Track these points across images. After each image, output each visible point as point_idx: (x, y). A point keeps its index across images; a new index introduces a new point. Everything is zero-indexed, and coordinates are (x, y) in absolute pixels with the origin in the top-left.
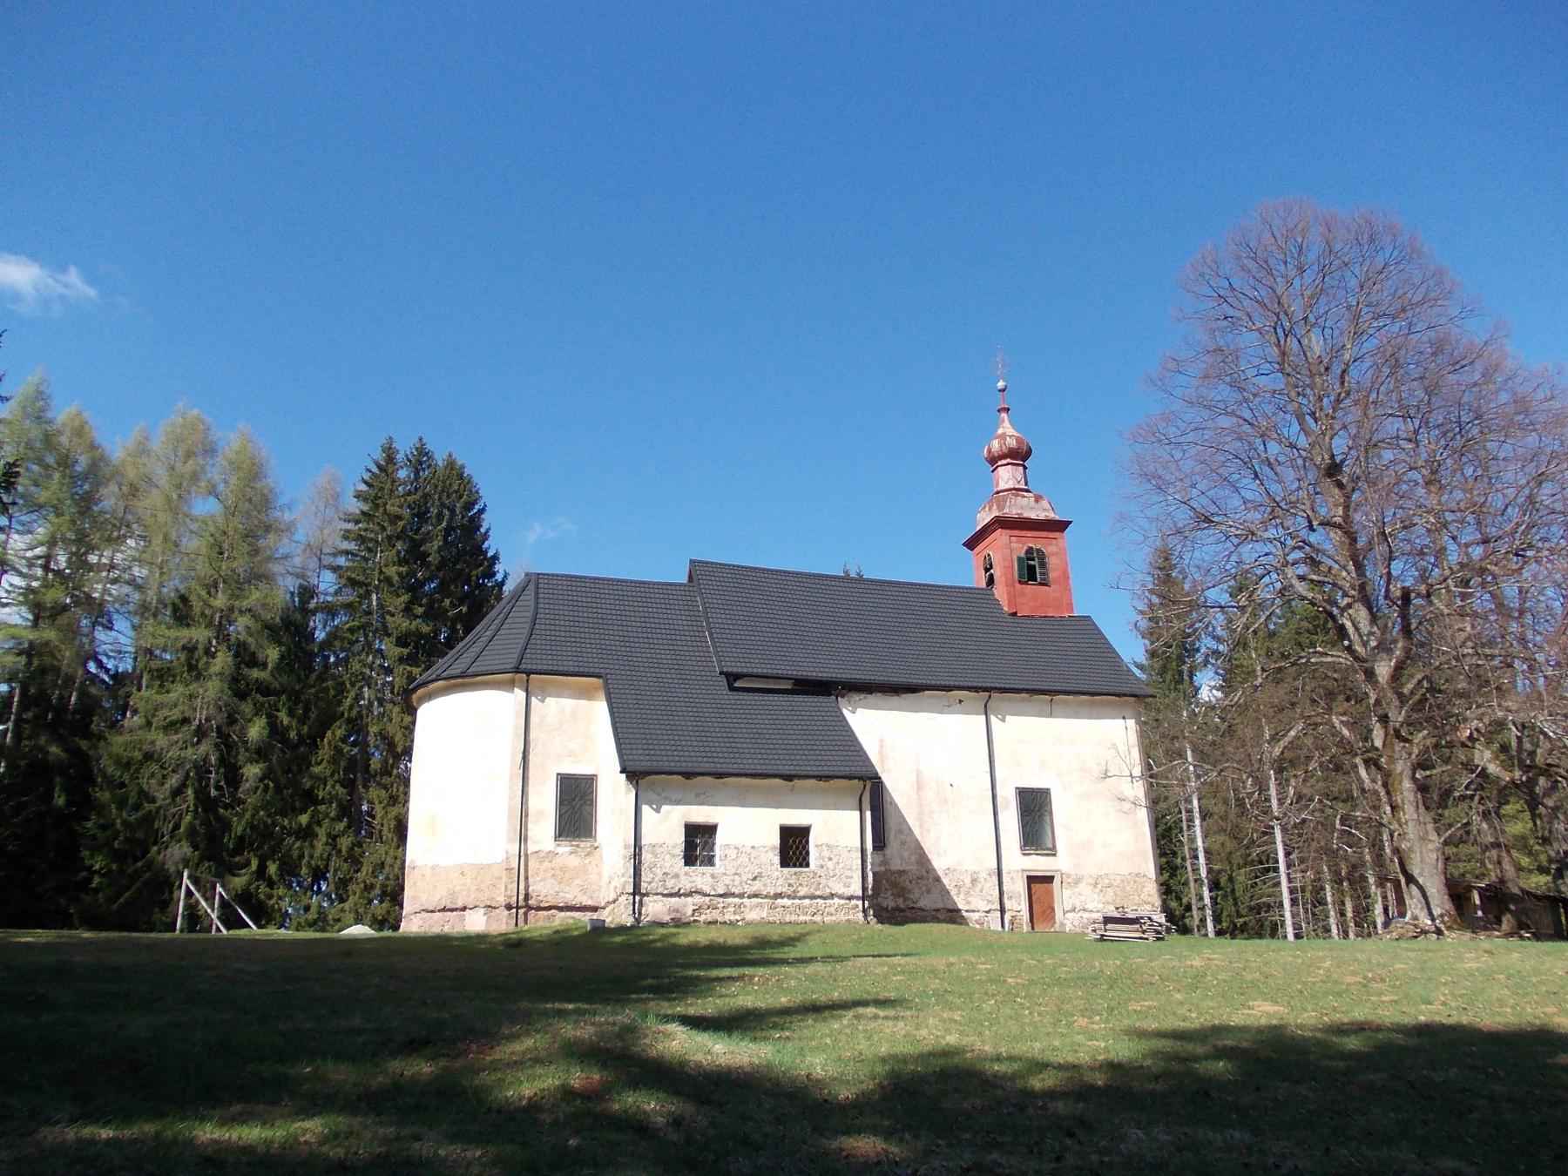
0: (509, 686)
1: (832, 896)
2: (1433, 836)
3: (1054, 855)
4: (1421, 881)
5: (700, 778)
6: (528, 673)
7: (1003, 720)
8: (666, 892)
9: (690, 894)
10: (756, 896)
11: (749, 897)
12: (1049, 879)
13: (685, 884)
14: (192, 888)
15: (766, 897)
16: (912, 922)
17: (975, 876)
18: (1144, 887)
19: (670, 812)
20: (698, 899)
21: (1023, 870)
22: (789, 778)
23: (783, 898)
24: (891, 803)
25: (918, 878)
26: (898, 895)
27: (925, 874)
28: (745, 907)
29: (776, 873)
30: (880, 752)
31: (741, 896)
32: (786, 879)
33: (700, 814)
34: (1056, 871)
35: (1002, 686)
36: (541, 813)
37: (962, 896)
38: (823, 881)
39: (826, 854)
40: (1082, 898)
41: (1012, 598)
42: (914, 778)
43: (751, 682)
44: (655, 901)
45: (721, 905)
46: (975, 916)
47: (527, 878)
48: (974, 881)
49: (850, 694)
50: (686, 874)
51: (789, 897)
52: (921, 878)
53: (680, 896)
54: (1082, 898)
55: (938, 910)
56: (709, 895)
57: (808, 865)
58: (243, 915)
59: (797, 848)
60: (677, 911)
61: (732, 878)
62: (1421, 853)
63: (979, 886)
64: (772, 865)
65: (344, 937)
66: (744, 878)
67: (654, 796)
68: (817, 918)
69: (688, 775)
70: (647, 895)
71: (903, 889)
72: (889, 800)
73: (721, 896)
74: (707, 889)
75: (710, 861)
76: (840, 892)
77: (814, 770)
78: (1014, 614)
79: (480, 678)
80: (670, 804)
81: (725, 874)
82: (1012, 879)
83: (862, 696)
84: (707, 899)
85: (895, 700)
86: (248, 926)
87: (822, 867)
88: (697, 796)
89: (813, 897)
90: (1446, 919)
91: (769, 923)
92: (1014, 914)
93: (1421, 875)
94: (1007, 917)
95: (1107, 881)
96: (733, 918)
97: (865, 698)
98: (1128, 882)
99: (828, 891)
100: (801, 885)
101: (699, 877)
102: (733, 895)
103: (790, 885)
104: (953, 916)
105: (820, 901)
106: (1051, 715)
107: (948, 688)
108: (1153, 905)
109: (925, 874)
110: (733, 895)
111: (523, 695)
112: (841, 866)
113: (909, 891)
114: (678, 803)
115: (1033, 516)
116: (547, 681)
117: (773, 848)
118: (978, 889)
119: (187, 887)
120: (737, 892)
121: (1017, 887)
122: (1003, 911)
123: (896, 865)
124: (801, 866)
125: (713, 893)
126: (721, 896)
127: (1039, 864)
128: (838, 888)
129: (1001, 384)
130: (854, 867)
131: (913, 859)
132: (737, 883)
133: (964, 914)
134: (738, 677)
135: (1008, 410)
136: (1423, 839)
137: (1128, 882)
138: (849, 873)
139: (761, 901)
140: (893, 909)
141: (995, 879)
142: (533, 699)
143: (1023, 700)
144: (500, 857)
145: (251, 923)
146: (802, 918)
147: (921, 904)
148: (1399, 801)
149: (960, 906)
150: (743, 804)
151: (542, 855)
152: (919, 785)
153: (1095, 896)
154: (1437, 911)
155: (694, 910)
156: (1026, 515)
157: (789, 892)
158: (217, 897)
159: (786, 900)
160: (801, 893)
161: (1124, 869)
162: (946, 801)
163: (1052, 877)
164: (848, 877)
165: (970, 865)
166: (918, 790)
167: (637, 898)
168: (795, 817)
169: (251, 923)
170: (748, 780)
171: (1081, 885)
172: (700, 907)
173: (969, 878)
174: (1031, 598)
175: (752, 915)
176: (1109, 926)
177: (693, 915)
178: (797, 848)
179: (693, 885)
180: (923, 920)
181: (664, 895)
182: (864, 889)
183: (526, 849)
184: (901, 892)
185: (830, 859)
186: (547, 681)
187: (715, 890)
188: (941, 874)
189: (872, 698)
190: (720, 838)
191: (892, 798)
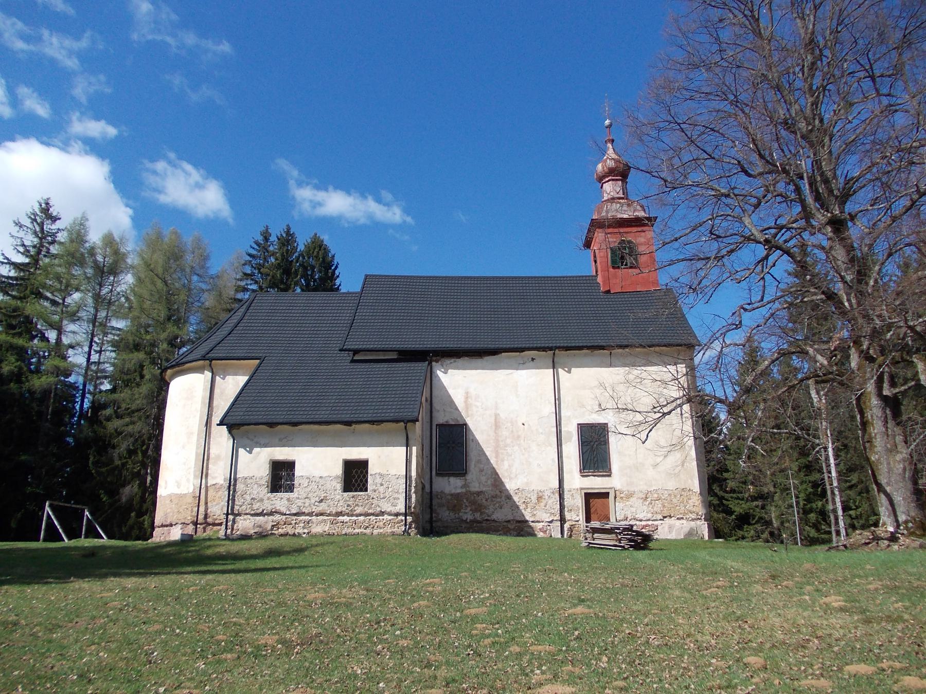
0: (200, 370)
1: (382, 513)
2: (901, 446)
3: (610, 476)
4: (888, 489)
5: (246, 427)
6: (211, 360)
7: (569, 372)
8: (252, 512)
9: (271, 513)
10: (322, 514)
11: (317, 515)
12: (606, 495)
13: (267, 506)
14: (50, 513)
15: (329, 515)
16: (453, 532)
17: (541, 494)
18: (690, 499)
19: (259, 453)
20: (277, 517)
21: (582, 489)
22: (348, 423)
23: (344, 516)
24: (473, 440)
25: (493, 497)
26: (475, 511)
27: (499, 494)
28: (313, 523)
29: (338, 497)
30: (466, 402)
31: (310, 514)
32: (346, 501)
33: (282, 453)
34: (611, 488)
35: (566, 345)
36: (218, 457)
37: (529, 510)
38: (375, 501)
39: (379, 480)
40: (633, 510)
41: (607, 280)
42: (492, 420)
43: (365, 355)
44: (245, 519)
45: (293, 522)
46: (540, 525)
47: (206, 503)
48: (539, 498)
49: (443, 359)
50: (268, 499)
51: (348, 515)
52: (496, 496)
53: (264, 515)
54: (633, 510)
55: (508, 521)
56: (285, 514)
57: (366, 490)
58: (99, 529)
59: (359, 477)
60: (260, 526)
61: (302, 501)
62: (889, 464)
63: (544, 502)
64: (336, 490)
65: (150, 545)
66: (313, 501)
67: (247, 441)
68: (368, 531)
69: (272, 425)
70: (239, 515)
71: (480, 506)
72: (471, 438)
73: (295, 515)
74: (284, 510)
75: (291, 489)
76: (388, 510)
77: (366, 417)
78: (608, 292)
79: (194, 363)
80: (261, 447)
81: (298, 498)
82: (572, 495)
83: (452, 360)
84: (284, 517)
85: (479, 362)
86: (103, 538)
87: (375, 491)
88: (280, 440)
89: (367, 515)
90: (910, 525)
91: (329, 535)
92: (574, 523)
93: (888, 484)
94: (566, 526)
95: (656, 496)
96: (301, 531)
97: (455, 361)
98: (675, 496)
99: (379, 509)
100: (357, 505)
101: (280, 501)
102: (303, 514)
103: (348, 506)
104: (521, 528)
105: (373, 518)
106: (611, 366)
107: (521, 350)
108: (697, 514)
109: (499, 494)
110: (303, 514)
111: (208, 374)
112: (390, 490)
113: (485, 508)
114: (266, 446)
115: (625, 216)
116: (227, 365)
117: (337, 477)
118: (542, 504)
119: (48, 513)
120: (306, 511)
121: (575, 503)
122: (563, 520)
123: (475, 487)
124: (361, 491)
125: (288, 513)
126: (295, 515)
127: (596, 483)
128: (387, 507)
129: (607, 122)
130: (401, 491)
131: (489, 482)
132: (307, 504)
133: (531, 524)
134: (356, 352)
135: (613, 141)
136: (893, 450)
137: (675, 496)
138: (396, 496)
139: (326, 518)
140: (471, 521)
141: (557, 496)
142: (217, 378)
143: (585, 355)
144: (191, 491)
145: (103, 535)
146: (357, 531)
147: (494, 517)
148: (869, 417)
149: (527, 518)
150: (315, 444)
151: (218, 486)
152: (497, 425)
153: (645, 508)
154: (902, 518)
155: (273, 526)
156: (619, 216)
157: (347, 511)
158: (85, 518)
159: (345, 517)
160: (358, 512)
161: (671, 485)
162: (519, 437)
163: (608, 493)
164: (395, 499)
165: (536, 486)
166: (496, 429)
167: (231, 517)
168: (356, 453)
169: (103, 535)
170: (316, 427)
171: (632, 499)
172: (278, 523)
173: (536, 496)
174: (623, 279)
175: (317, 529)
176: (596, 535)
177: (272, 529)
178: (359, 477)
179: (273, 507)
180: (487, 531)
181: (252, 515)
182: (407, 507)
183: (206, 483)
184: (478, 508)
185: (382, 485)
186: (227, 365)
187: (289, 510)
188: (512, 493)
189: (460, 361)
190: (298, 471)
191: (473, 435)
